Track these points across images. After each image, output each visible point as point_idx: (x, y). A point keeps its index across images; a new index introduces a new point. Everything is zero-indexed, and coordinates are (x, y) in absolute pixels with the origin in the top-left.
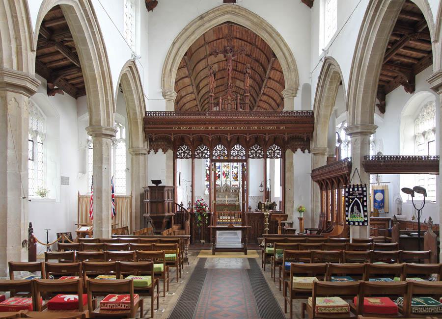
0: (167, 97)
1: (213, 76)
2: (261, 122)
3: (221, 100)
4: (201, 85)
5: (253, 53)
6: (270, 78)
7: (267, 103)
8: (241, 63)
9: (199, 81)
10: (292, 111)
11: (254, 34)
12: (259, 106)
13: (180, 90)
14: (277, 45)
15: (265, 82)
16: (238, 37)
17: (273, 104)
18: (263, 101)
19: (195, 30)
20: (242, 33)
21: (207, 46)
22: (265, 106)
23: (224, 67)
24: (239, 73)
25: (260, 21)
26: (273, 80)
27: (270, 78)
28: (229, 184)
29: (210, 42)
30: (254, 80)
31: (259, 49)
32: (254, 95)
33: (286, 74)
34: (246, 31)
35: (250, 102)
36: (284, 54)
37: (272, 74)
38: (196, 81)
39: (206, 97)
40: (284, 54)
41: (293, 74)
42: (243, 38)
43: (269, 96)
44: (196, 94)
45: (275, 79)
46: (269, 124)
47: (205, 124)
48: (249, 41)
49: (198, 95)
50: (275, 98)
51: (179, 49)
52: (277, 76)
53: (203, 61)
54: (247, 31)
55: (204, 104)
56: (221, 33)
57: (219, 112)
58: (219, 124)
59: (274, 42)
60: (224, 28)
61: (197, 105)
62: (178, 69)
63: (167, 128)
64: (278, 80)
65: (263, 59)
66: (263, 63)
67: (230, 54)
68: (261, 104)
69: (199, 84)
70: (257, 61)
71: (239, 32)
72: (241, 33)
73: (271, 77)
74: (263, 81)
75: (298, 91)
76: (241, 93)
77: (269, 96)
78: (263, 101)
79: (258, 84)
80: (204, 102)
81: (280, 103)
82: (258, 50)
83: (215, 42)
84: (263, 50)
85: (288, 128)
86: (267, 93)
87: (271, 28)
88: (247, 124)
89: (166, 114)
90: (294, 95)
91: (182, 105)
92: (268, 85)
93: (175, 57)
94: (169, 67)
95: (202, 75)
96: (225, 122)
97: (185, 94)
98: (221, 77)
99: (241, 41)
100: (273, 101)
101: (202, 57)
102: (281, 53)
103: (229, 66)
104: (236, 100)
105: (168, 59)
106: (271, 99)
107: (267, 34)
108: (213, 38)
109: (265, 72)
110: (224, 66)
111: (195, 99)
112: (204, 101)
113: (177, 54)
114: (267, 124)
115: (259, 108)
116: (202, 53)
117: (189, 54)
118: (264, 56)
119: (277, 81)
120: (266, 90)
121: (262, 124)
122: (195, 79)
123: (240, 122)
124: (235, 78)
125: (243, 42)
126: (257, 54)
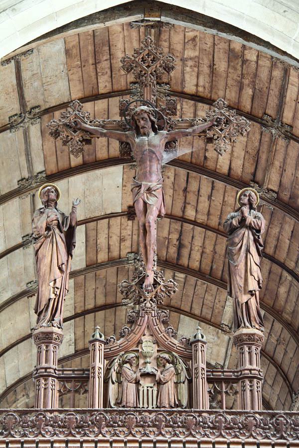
3: (100, 364)
5: (270, 164)
8: (206, 227)
16: (190, 88)
20: (212, 66)
21: (35, 130)
23: (115, 254)
24: (192, 280)
28: (257, 112)
34: (233, 56)
56: (105, 65)
72: (206, 69)
98: (101, 301)
103: (149, 190)
110: (115, 240)
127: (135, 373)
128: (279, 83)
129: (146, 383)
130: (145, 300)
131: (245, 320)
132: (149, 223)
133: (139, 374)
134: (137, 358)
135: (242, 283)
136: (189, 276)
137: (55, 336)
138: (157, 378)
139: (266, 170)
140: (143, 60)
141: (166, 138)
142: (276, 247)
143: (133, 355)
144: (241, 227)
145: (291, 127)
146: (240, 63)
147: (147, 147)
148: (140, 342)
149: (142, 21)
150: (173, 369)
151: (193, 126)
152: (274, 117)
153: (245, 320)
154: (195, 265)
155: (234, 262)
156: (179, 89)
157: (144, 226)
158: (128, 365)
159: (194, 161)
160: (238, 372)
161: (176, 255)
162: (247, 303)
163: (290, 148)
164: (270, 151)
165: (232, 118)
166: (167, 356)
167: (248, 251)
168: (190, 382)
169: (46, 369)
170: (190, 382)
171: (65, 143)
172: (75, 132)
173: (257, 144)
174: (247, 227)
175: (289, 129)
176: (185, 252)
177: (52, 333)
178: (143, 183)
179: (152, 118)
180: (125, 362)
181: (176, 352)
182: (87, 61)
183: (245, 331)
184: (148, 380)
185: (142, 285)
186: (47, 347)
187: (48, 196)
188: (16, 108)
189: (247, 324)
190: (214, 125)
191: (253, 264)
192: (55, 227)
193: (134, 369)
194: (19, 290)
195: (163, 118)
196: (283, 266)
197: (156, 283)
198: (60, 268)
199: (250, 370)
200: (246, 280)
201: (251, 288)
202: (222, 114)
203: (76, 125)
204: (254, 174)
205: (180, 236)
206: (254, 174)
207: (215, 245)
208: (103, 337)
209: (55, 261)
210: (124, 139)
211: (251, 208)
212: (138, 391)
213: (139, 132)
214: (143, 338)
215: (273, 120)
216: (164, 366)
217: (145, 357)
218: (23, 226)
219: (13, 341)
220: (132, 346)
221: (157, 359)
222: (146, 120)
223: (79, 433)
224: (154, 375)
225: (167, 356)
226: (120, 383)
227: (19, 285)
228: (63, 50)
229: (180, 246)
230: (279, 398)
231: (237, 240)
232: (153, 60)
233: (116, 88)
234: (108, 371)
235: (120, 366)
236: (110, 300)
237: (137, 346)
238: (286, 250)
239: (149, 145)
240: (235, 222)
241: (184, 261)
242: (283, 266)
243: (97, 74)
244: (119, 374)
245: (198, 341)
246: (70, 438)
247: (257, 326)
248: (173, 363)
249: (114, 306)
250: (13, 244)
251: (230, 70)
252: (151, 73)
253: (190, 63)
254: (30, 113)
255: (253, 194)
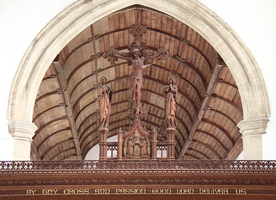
0: (16, 134)
1: (107, 96)
2: (198, 180)
4: (82, 104)
6: (214, 95)
7: (212, 136)
9: (79, 96)
10: (258, 161)
11: (183, 24)
12: (194, 141)
13: (40, 114)
14: (225, 45)
15: (206, 100)
16: (154, 26)
17: (223, 137)
18: (204, 132)
19: (77, 19)
20: (161, 22)
21: (97, 42)
22: (207, 140)
23: (126, 74)
25: (194, 5)
26: (221, 98)
27: (214, 95)
29: (101, 36)
30: (185, 95)
31: (194, 47)
32: (186, 120)
33: (244, 93)
35: (177, 132)
36: (239, 60)
37: (219, 89)
38: (73, 97)
39: (91, 122)
40: (239, 60)
41: (258, 94)
42: (164, 30)
43: (214, 124)
44: (72, 119)
45: (226, 96)
46: (216, 184)
47: (91, 183)
48: (174, 34)
49: (75, 120)
50: (225, 128)
51: (45, 50)
52: (228, 92)
53: (89, 64)
54: (170, 20)
55: (86, 134)
56: (123, 21)
57: (116, 160)
58: (117, 184)
59: (221, 40)
60: (128, 15)
61: (72, 138)
62: (44, 79)
63: (14, 192)
64: (231, 99)
65: (200, 62)
66: (200, 69)
67: (140, 61)
68: (200, 136)
69: (78, 101)
70: (190, 65)
71: (156, 20)
73: (217, 93)
74: (202, 99)
75: (268, 124)
76: (159, 115)
77: (214, 124)
78: (204, 132)
79: (193, 103)
80: (85, 131)
81: (236, 140)
82: (191, 49)
83: (112, 35)
84: (201, 49)
85: (252, 192)
86: (211, 119)
87: (215, 16)
88: (172, 183)
89: (13, 165)
90: (261, 130)
91: (43, 138)
92: (211, 105)
93: (37, 64)
94: (24, 81)
95: (85, 86)
96: (130, 180)
97: (49, 120)
98: (121, 88)
99: (158, 34)
100: (221, 132)
101: (87, 57)
102: (234, 57)
103: (138, 80)
104: (151, 138)
105: (23, 68)
106: (218, 130)
107: (207, 27)
108: (106, 29)
109: (206, 84)
111: (69, 128)
112: (88, 134)
113: (40, 58)
114: (209, 183)
115: (195, 143)
116: (87, 52)
117: (62, 58)
118: (203, 58)
119: (227, 100)
120: (208, 114)
121: (200, 184)
122: (71, 95)
123: (158, 180)
124: (147, 90)
125: (163, 36)
126: (188, 53)
127: (133, 143)
128: (185, 29)
129: (136, 147)
130: (136, 118)
131: (170, 125)
132: (138, 92)
133: (134, 144)
134: (134, 138)
135: (169, 112)
136: (154, 82)
137: (106, 131)
138: (140, 145)
139: (182, 53)
140: (136, 30)
141: (144, 60)
142: (186, 76)
143: (132, 137)
144: (169, 92)
145: (190, 42)
146: (171, 22)
147: (137, 64)
148: (134, 133)
149: (136, 9)
150: (145, 142)
151: (153, 55)
152: (184, 38)
153: (170, 125)
154: (157, 78)
155: (167, 104)
156: (150, 27)
157: (136, 93)
158: (130, 141)
159: (155, 47)
160: (167, 143)
161: (149, 74)
162: (171, 119)
163: (190, 47)
164: (183, 48)
165: (167, 52)
166: (143, 138)
167: (171, 100)
168: (151, 146)
169: (103, 142)
170: (151, 146)
171: (109, 61)
172: (112, 57)
173: (178, 45)
174: (171, 92)
175: (189, 42)
176: (153, 74)
177: (105, 130)
178: (136, 77)
179: (139, 53)
180: (129, 140)
181: (147, 136)
182: (116, 20)
183: (170, 129)
184: (137, 145)
185: (135, 113)
186: (103, 135)
187: (103, 81)
188: (90, 36)
189: (171, 126)
190: (161, 55)
191: (173, 104)
192: (106, 92)
193: (132, 142)
194: (90, 88)
195: (143, 52)
196: (188, 82)
197: (140, 112)
198: (107, 107)
199: (171, 142)
200: (171, 111)
201: (172, 114)
202: (164, 51)
203: (113, 55)
204: (178, 53)
205: (151, 69)
206: (178, 53)
207: (164, 72)
208: (122, 131)
209: (106, 105)
210: (129, 60)
211: (173, 84)
212: (134, 149)
213: (134, 58)
214: (135, 131)
215: (183, 39)
216: (142, 141)
217: (136, 138)
218: (92, 69)
219: (88, 104)
220: (131, 134)
221: (140, 138)
222: (137, 54)
223: (114, 168)
224: (139, 144)
225: (143, 138)
226: (128, 147)
227: (90, 86)
228: (108, 19)
229: (151, 72)
230: (188, 122)
231: (168, 96)
232: (140, 30)
233: (126, 27)
234: (123, 143)
235: (128, 141)
236: (125, 88)
237: (134, 134)
238: (190, 77)
239: (138, 63)
240: (167, 90)
241: (153, 76)
242: (188, 82)
243: (120, 24)
244: (127, 144)
245: (154, 133)
246: (112, 169)
247: (174, 127)
248: (145, 140)
249: (126, 89)
250: (88, 75)
251: (168, 23)
252: (139, 35)
253: (153, 20)
254: (95, 37)
255: (174, 79)
